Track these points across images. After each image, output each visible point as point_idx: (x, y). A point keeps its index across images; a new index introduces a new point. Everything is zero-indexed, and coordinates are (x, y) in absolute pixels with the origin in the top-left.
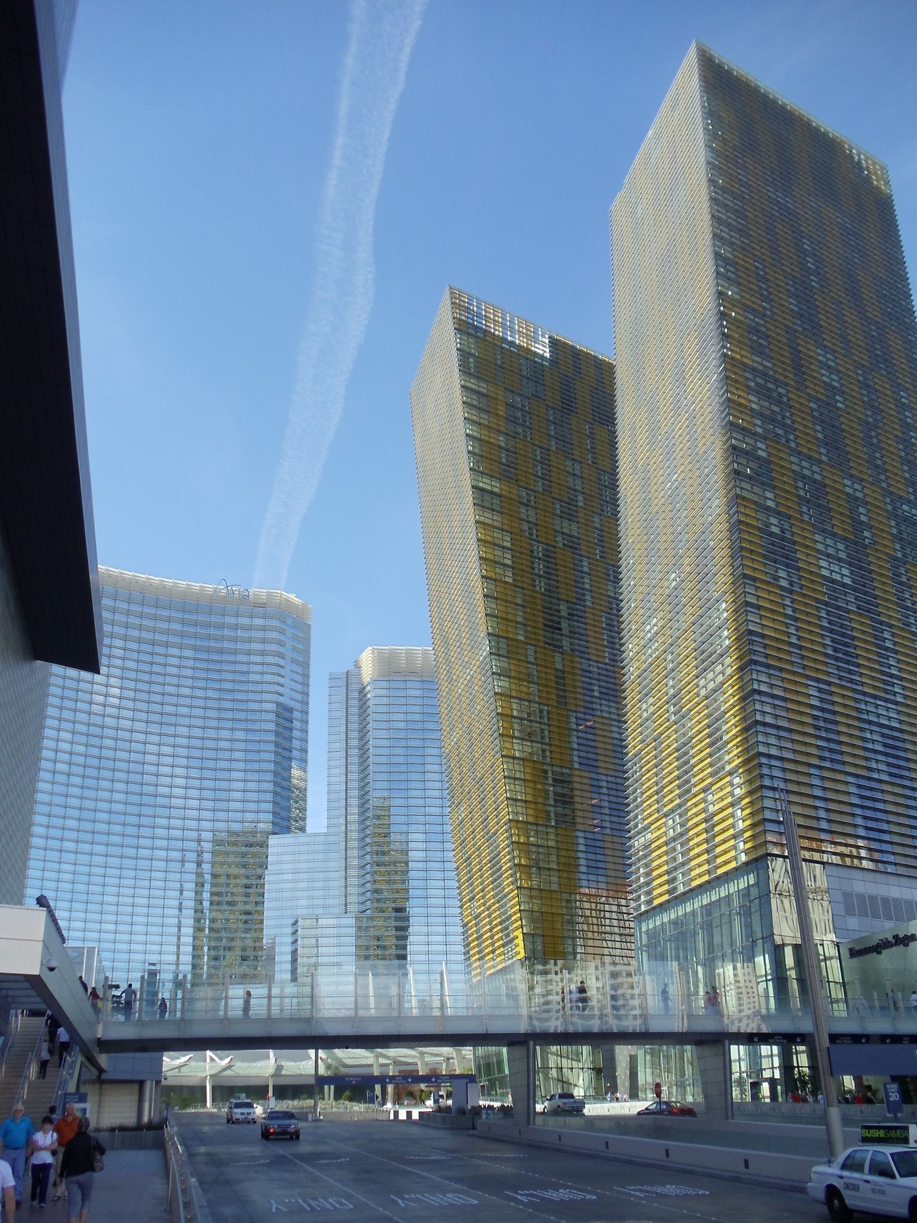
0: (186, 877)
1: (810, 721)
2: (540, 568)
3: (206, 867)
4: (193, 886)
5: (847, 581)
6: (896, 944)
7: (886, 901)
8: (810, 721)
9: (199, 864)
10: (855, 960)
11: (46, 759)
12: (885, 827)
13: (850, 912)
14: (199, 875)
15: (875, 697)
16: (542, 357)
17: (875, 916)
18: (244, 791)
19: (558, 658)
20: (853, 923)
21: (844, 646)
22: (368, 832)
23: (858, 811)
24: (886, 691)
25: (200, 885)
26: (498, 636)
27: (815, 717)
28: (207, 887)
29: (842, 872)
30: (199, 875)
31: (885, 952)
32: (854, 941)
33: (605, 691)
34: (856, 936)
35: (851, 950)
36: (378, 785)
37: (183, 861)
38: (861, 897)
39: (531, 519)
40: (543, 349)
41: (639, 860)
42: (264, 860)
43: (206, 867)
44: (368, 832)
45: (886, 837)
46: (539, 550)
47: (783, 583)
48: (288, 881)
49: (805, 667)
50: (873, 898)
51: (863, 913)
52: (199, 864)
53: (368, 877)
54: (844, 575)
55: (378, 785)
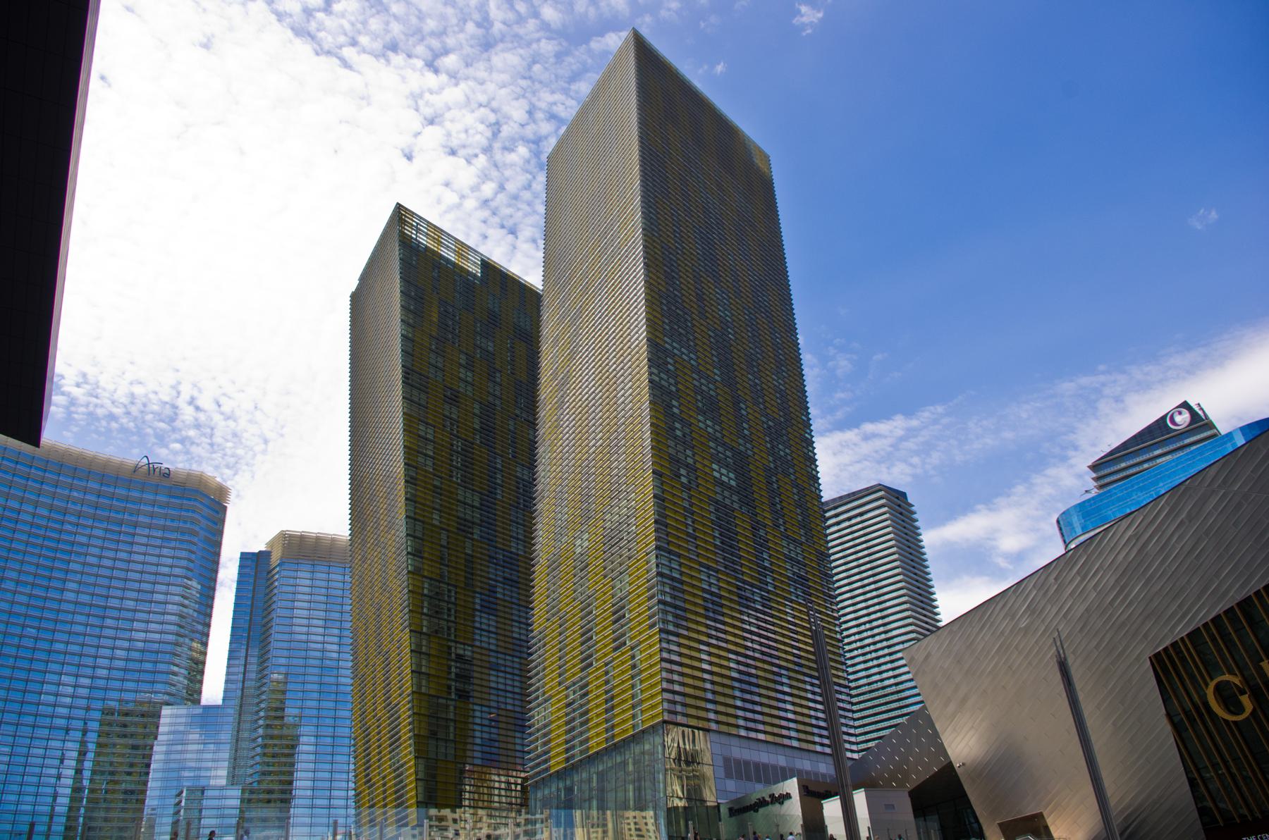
0: (69, 745)
1: (700, 602)
2: (458, 461)
3: (92, 737)
4: (75, 754)
5: (733, 483)
6: (772, 803)
7: (757, 765)
8: (700, 602)
9: (85, 732)
10: (1029, 812)
11: (57, 406)
12: (757, 699)
13: (728, 775)
14: (83, 743)
15: (752, 585)
16: (475, 275)
17: (749, 779)
18: (110, 669)
19: (468, 544)
20: (731, 785)
21: (729, 541)
22: (263, 705)
23: (737, 684)
24: (760, 581)
25: (82, 754)
26: (415, 519)
27: (705, 599)
28: (91, 755)
29: (724, 739)
30: (83, 743)
31: (761, 810)
32: (732, 801)
33: (488, 756)
34: (733, 797)
35: (730, 810)
36: (279, 653)
37: (67, 730)
38: (738, 762)
39: (454, 416)
40: (477, 271)
41: (538, 730)
42: (153, 729)
43: (92, 737)
44: (263, 705)
45: (758, 708)
46: (458, 445)
47: (684, 480)
48: (192, 752)
49: (698, 555)
50: (747, 763)
51: (739, 777)
52: (85, 732)
53: (259, 750)
54: (729, 478)
55: (279, 653)
